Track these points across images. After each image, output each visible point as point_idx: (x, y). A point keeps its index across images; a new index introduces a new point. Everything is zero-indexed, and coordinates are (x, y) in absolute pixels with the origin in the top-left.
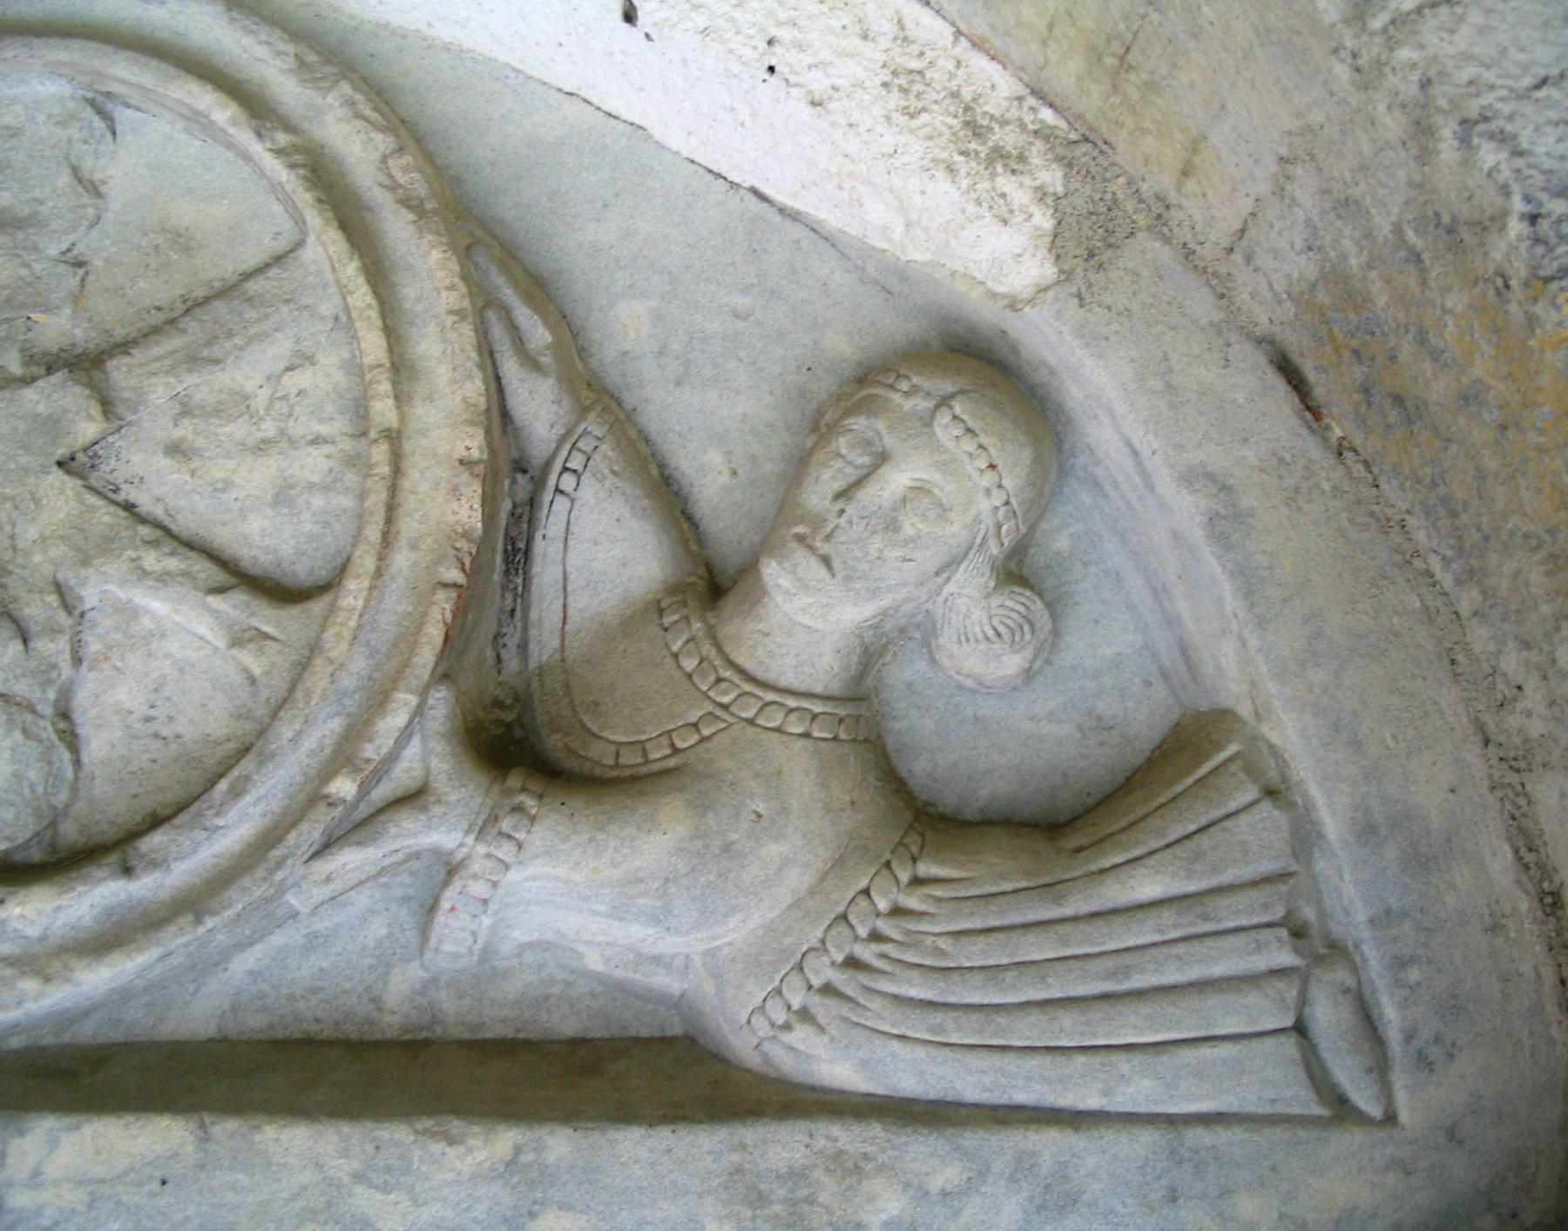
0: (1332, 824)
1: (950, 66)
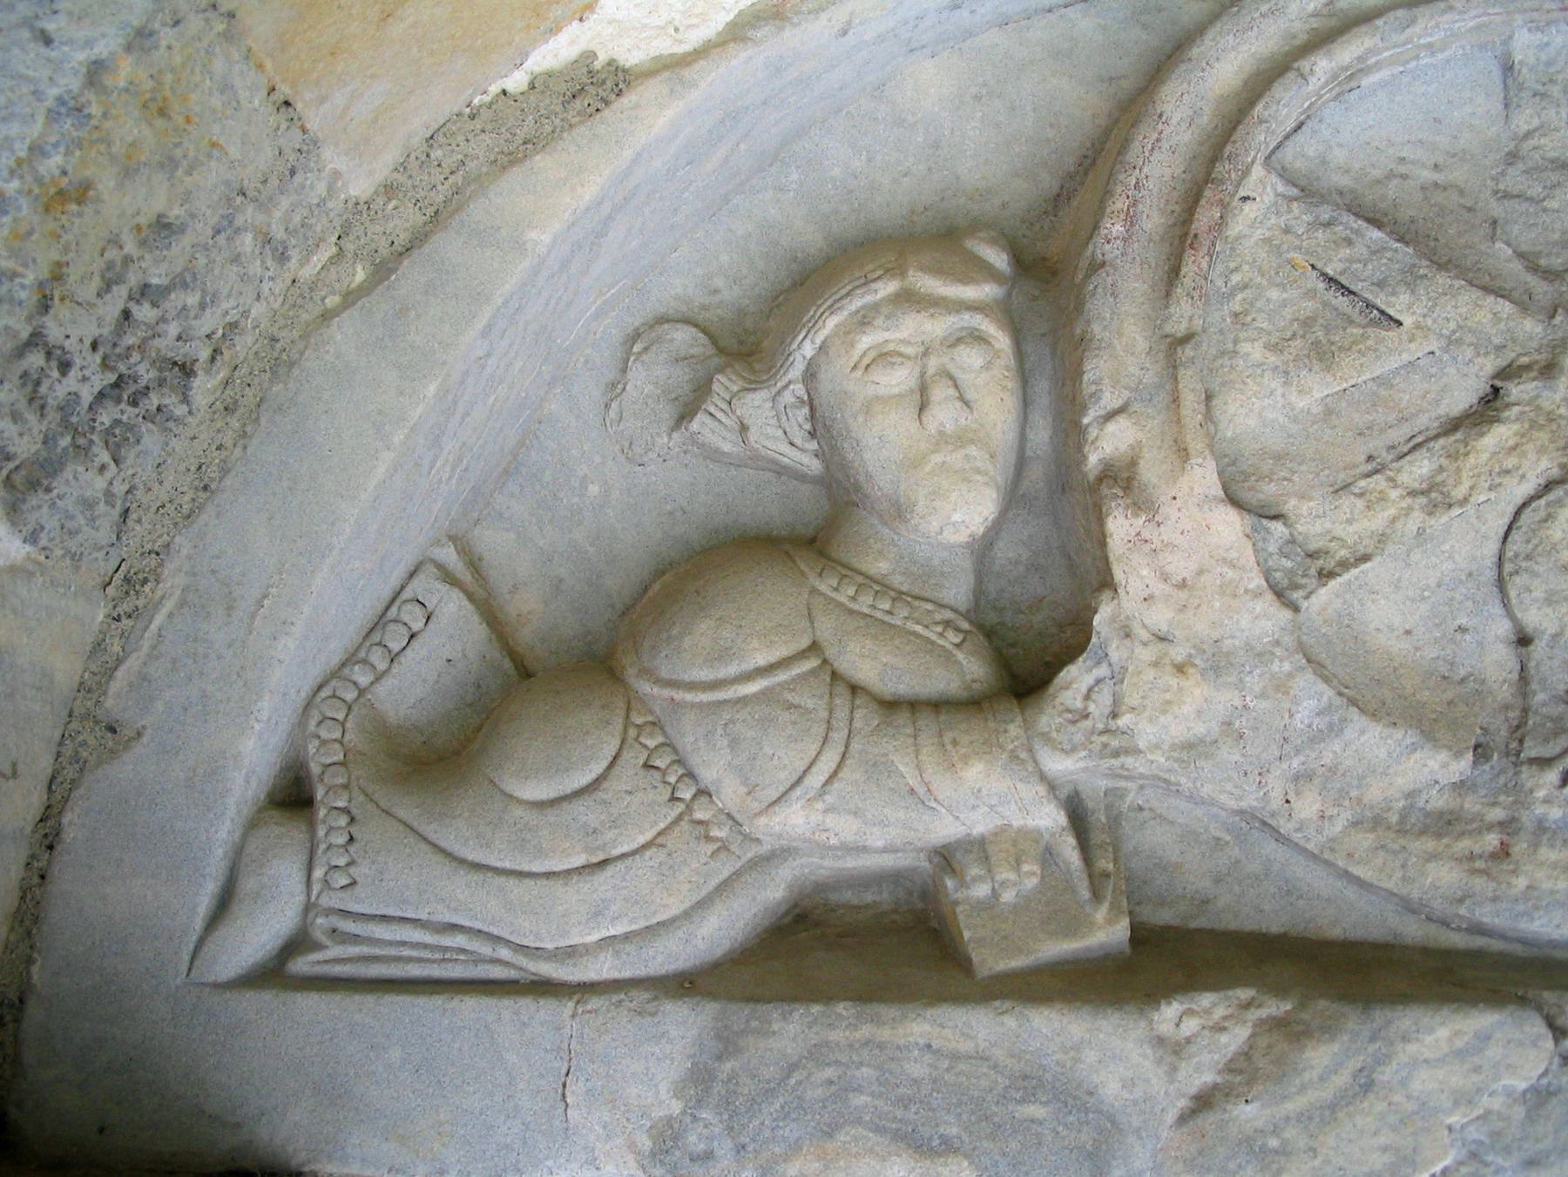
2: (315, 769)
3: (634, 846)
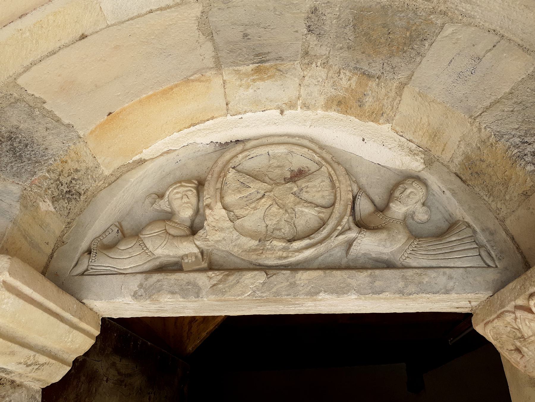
0: (478, 230)
1: (407, 144)
2: (92, 248)
3: (136, 255)
